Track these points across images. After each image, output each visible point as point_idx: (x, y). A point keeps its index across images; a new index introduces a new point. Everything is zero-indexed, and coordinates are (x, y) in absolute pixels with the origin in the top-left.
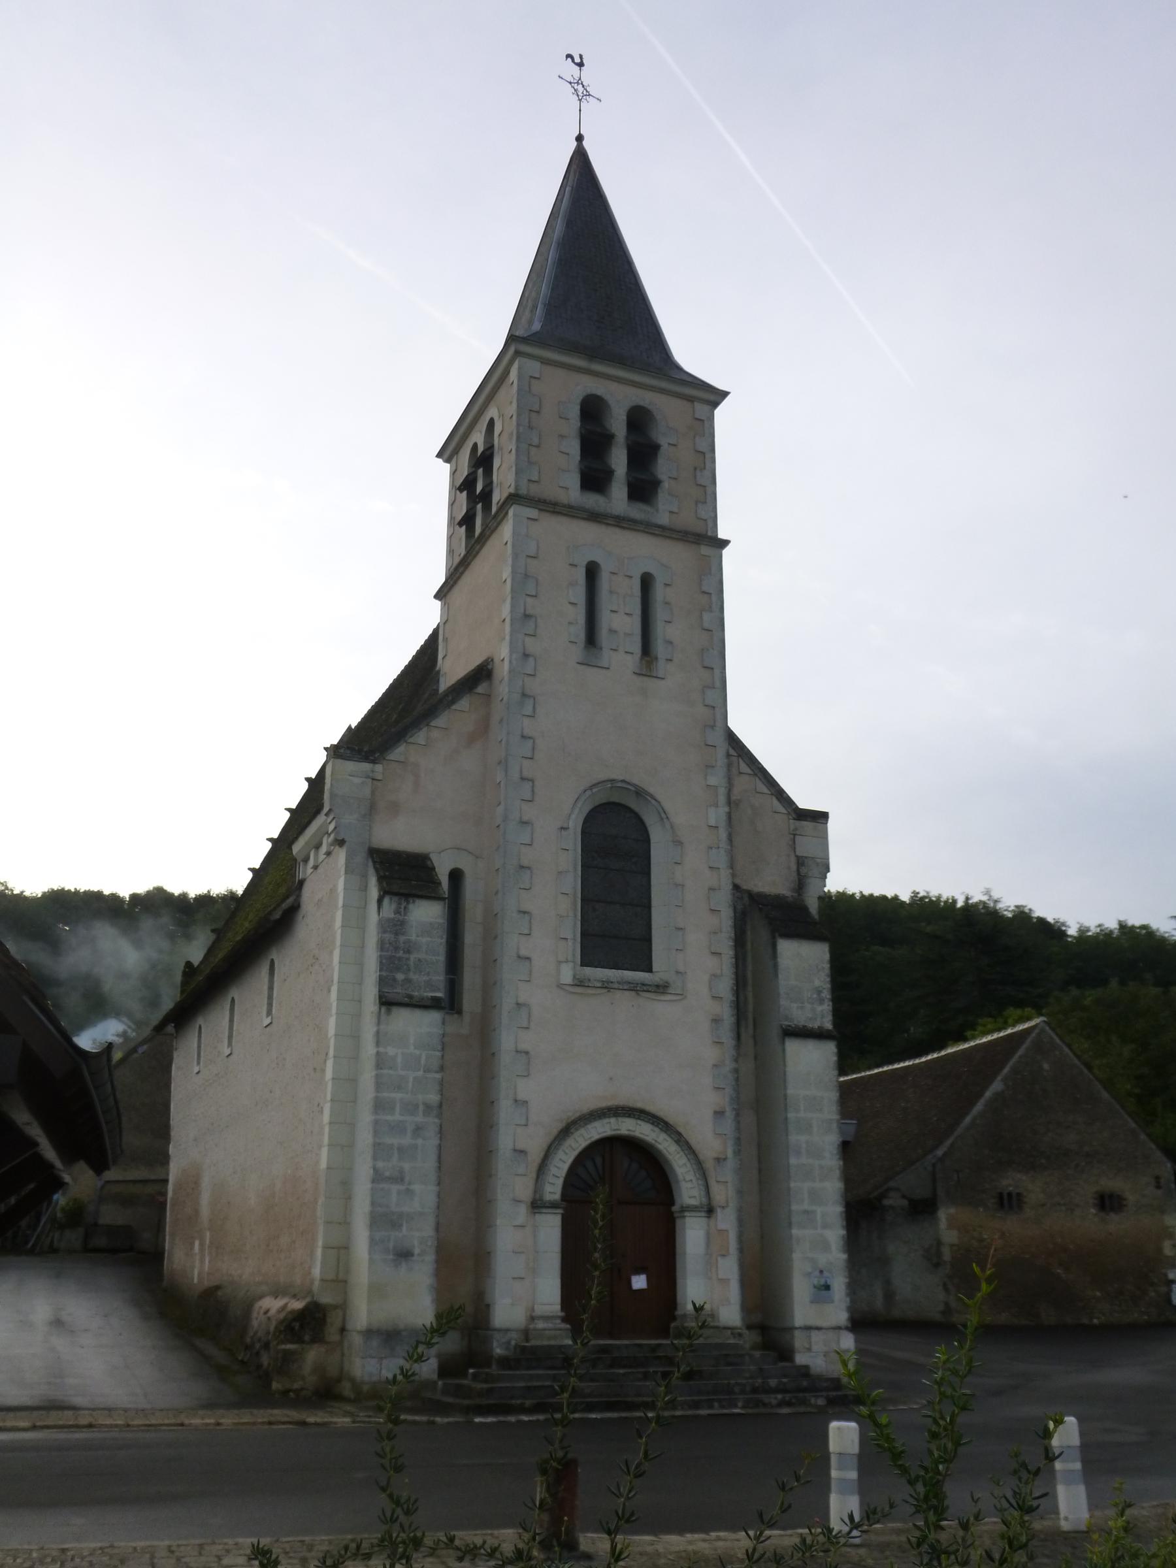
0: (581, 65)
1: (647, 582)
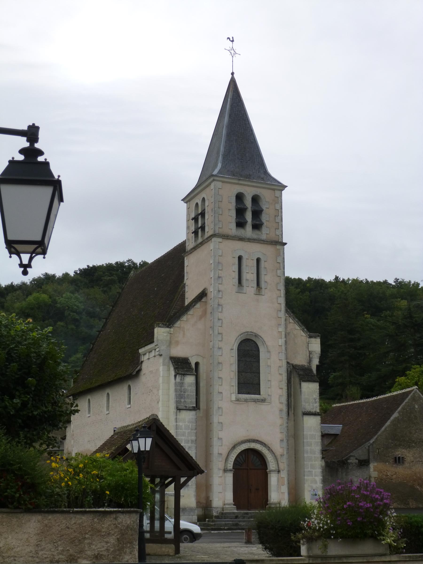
0: (233, 41)
1: (258, 260)
